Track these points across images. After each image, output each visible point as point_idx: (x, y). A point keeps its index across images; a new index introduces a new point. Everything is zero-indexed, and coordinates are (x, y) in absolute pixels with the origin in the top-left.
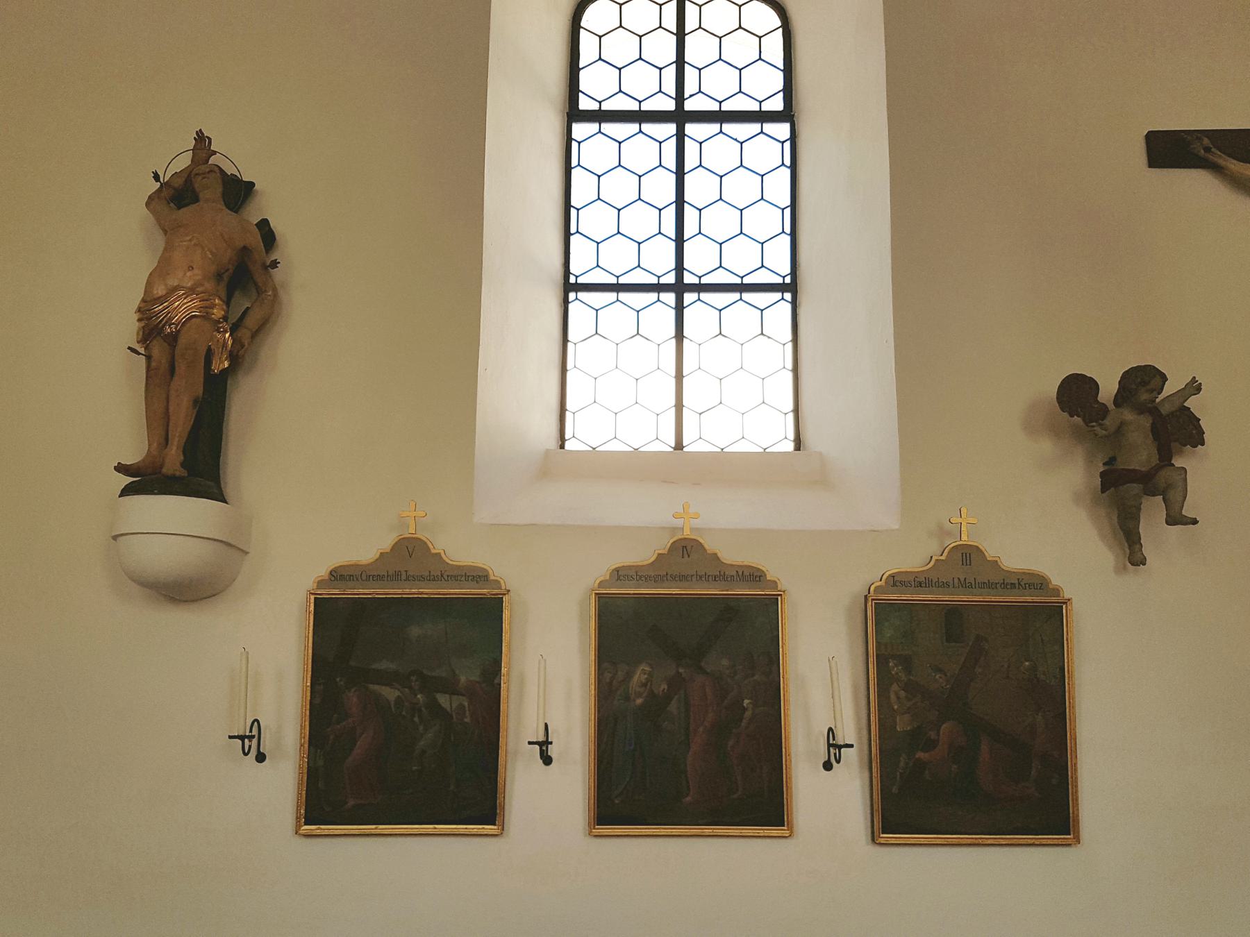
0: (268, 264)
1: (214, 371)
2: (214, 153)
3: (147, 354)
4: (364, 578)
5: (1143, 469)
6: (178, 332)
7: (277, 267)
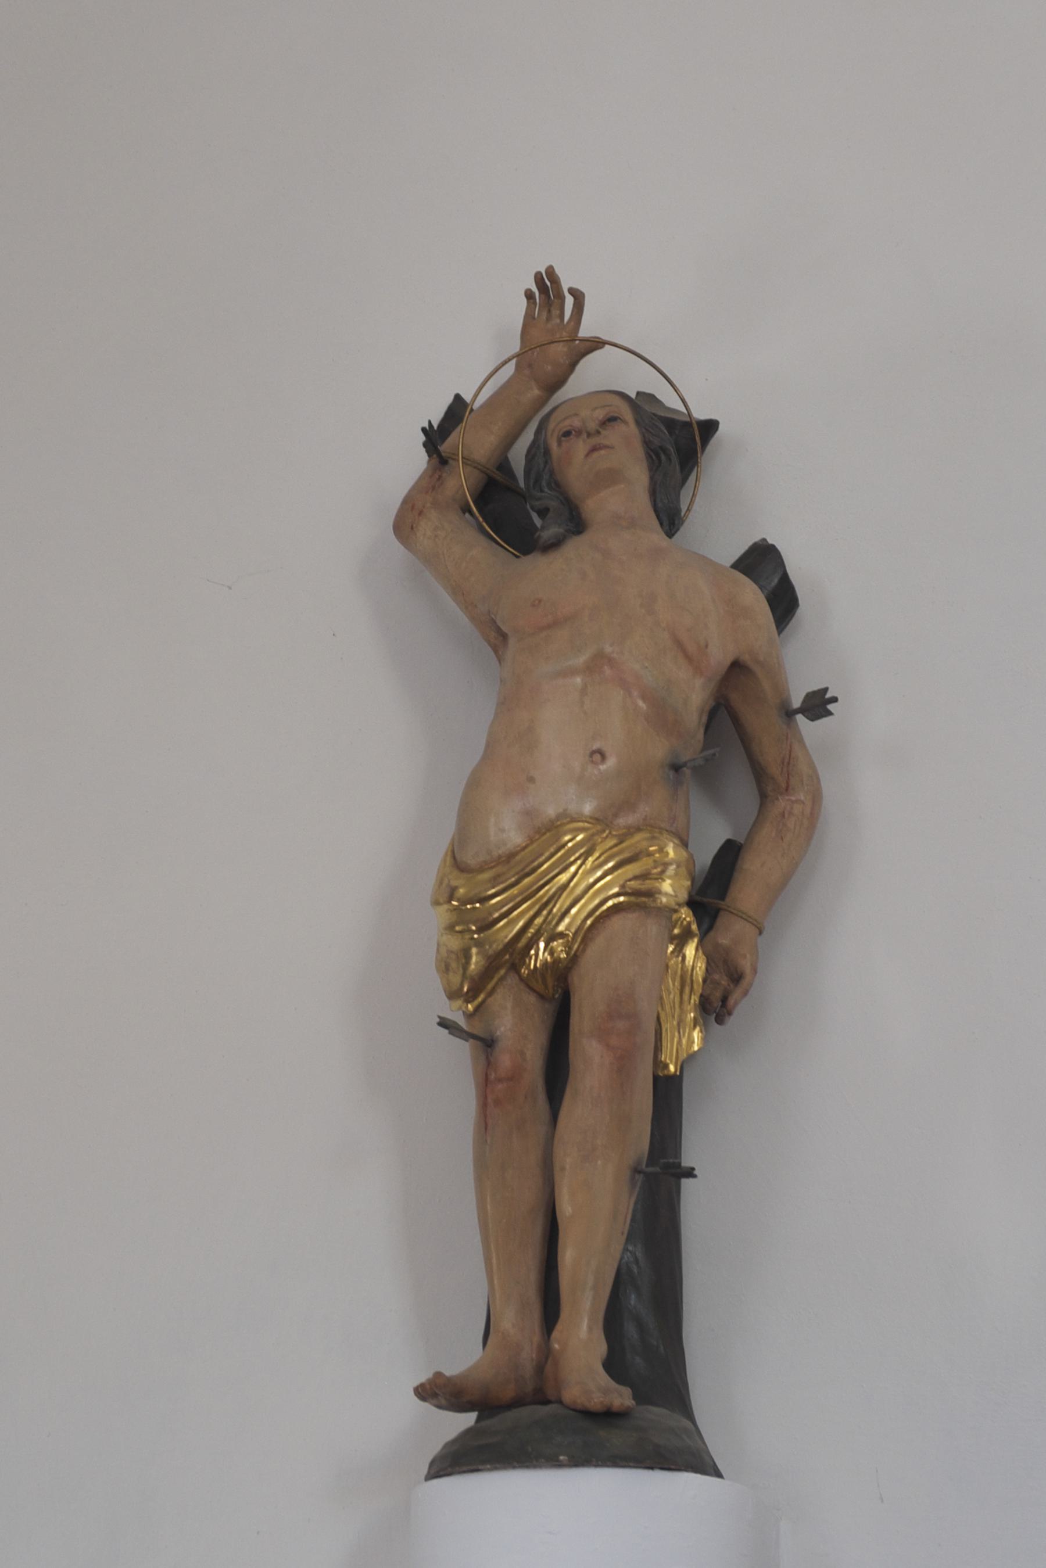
0: (797, 702)
1: (666, 1066)
2: (596, 344)
3: (477, 1031)
5: (622, 692)
6: (574, 959)
7: (830, 713)
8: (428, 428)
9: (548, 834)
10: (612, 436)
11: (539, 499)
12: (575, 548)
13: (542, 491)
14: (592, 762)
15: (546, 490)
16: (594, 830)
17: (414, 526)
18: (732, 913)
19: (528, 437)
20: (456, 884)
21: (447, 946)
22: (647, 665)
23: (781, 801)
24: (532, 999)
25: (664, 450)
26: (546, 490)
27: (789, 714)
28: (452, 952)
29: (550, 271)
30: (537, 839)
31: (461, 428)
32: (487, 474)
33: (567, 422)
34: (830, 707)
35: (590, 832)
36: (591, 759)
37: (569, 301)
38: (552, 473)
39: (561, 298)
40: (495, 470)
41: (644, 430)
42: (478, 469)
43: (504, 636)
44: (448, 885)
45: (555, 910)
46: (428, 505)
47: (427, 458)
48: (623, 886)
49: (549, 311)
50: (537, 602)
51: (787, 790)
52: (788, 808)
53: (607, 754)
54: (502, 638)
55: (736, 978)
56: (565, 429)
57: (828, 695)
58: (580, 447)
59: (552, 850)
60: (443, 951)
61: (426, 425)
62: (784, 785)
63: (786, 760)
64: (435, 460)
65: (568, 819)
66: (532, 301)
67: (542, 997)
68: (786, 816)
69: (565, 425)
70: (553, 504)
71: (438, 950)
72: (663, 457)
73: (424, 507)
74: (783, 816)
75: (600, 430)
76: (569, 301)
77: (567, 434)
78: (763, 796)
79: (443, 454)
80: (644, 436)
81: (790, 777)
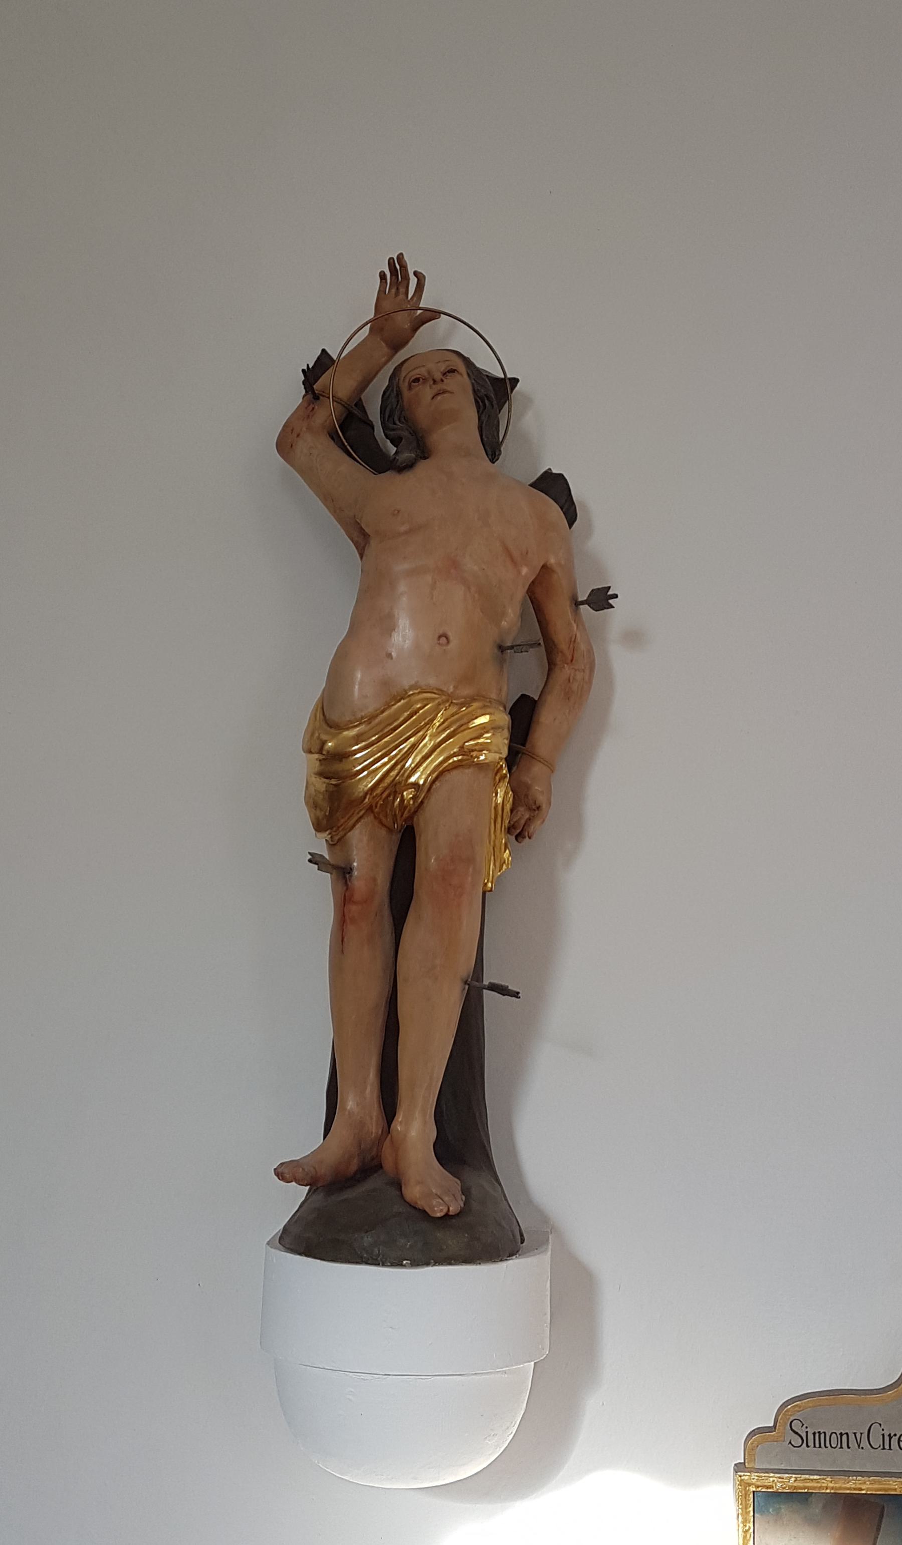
0: (582, 597)
2: (433, 314)
4: (876, 1441)
7: (612, 607)
8: (306, 370)
9: (402, 701)
10: (451, 383)
11: (393, 430)
12: (422, 467)
13: (395, 424)
14: (439, 644)
15: (397, 422)
16: (440, 700)
17: (293, 445)
18: (531, 757)
19: (381, 382)
20: (326, 739)
21: (315, 786)
22: (484, 567)
23: (567, 669)
24: (383, 832)
25: (488, 398)
26: (397, 422)
27: (577, 604)
28: (320, 792)
29: (401, 254)
30: (393, 705)
31: (333, 369)
32: (348, 410)
33: (417, 371)
34: (611, 601)
35: (437, 702)
36: (438, 642)
37: (413, 281)
38: (402, 409)
39: (406, 278)
40: (353, 407)
41: (473, 381)
42: (342, 404)
43: (365, 536)
44: (319, 738)
45: (407, 765)
46: (304, 429)
47: (304, 392)
48: (462, 747)
49: (397, 289)
50: (397, 512)
51: (572, 661)
52: (572, 675)
53: (451, 638)
54: (363, 537)
55: (536, 809)
56: (415, 377)
57: (610, 593)
58: (427, 392)
59: (406, 714)
60: (312, 789)
61: (305, 368)
62: (570, 657)
63: (573, 640)
64: (310, 396)
65: (419, 690)
66: (383, 281)
67: (390, 830)
68: (571, 681)
69: (414, 374)
70: (405, 434)
71: (307, 787)
72: (487, 402)
73: (301, 430)
74: (569, 680)
75: (443, 379)
76: (413, 281)
77: (417, 380)
78: (551, 665)
79: (316, 392)
80: (473, 386)
81: (575, 652)
